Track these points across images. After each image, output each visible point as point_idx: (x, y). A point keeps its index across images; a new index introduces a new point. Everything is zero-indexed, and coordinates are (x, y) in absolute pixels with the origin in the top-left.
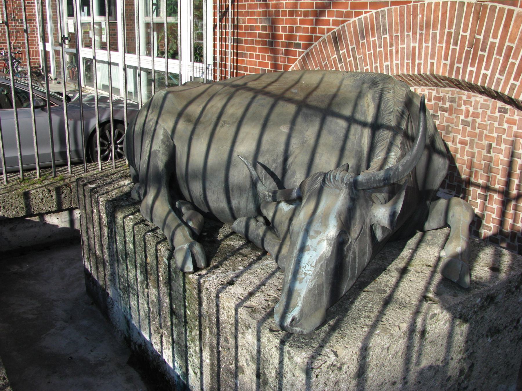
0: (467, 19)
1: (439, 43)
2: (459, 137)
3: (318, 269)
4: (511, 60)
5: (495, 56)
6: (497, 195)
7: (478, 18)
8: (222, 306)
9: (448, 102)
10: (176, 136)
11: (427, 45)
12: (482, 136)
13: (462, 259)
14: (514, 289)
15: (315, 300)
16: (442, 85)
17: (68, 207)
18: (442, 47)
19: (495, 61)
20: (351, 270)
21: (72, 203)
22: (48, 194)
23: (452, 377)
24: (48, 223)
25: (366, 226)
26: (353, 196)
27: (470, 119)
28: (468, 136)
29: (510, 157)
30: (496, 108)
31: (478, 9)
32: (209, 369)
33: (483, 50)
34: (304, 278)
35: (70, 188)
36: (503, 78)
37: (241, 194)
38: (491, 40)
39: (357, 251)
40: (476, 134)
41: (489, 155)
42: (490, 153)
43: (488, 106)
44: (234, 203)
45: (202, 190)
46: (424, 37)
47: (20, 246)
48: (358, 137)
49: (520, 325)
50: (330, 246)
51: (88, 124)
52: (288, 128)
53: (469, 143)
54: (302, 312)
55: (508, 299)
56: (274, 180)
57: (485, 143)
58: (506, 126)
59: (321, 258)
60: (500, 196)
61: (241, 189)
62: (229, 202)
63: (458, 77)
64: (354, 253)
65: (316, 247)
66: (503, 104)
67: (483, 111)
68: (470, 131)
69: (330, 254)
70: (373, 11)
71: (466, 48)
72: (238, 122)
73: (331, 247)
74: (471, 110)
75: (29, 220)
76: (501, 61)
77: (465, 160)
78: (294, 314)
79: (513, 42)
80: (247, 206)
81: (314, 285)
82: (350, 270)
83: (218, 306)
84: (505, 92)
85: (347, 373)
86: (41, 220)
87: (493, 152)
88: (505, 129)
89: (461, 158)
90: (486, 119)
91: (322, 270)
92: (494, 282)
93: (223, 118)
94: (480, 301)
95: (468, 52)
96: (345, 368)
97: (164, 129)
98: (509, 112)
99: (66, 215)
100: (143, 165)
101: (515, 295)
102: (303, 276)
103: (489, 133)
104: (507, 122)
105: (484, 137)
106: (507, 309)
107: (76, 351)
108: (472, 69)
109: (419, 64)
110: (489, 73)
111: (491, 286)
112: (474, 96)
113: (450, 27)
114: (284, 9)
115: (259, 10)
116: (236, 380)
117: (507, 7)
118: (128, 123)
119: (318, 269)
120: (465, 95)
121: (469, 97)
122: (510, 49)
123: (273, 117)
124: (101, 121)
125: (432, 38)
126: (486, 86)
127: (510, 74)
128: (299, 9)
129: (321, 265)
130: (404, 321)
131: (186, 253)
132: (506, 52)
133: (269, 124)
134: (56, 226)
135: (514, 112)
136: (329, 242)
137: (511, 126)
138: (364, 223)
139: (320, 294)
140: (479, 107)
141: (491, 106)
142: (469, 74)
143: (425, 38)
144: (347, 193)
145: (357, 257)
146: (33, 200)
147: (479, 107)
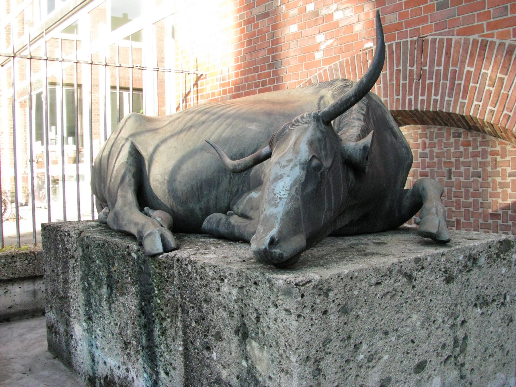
0: (412, 55)
3: (293, 192)
4: (457, 82)
5: (442, 81)
14: (495, 256)
23: (447, 346)
28: (428, 167)
33: (431, 78)
36: (452, 99)
39: (331, 180)
40: (435, 163)
41: (450, 180)
50: (304, 170)
53: (429, 173)
54: (280, 232)
57: (445, 170)
58: (462, 149)
67: (439, 140)
69: (304, 178)
76: (448, 84)
80: (216, 204)
81: (291, 208)
82: (326, 199)
84: (456, 111)
88: (462, 152)
90: (442, 147)
91: (297, 194)
96: (331, 295)
103: (447, 159)
104: (463, 145)
108: (423, 98)
110: (438, 98)
113: (398, 65)
117: (445, 37)
120: (420, 129)
129: (297, 189)
137: (466, 148)
140: (434, 137)
147: (434, 137)
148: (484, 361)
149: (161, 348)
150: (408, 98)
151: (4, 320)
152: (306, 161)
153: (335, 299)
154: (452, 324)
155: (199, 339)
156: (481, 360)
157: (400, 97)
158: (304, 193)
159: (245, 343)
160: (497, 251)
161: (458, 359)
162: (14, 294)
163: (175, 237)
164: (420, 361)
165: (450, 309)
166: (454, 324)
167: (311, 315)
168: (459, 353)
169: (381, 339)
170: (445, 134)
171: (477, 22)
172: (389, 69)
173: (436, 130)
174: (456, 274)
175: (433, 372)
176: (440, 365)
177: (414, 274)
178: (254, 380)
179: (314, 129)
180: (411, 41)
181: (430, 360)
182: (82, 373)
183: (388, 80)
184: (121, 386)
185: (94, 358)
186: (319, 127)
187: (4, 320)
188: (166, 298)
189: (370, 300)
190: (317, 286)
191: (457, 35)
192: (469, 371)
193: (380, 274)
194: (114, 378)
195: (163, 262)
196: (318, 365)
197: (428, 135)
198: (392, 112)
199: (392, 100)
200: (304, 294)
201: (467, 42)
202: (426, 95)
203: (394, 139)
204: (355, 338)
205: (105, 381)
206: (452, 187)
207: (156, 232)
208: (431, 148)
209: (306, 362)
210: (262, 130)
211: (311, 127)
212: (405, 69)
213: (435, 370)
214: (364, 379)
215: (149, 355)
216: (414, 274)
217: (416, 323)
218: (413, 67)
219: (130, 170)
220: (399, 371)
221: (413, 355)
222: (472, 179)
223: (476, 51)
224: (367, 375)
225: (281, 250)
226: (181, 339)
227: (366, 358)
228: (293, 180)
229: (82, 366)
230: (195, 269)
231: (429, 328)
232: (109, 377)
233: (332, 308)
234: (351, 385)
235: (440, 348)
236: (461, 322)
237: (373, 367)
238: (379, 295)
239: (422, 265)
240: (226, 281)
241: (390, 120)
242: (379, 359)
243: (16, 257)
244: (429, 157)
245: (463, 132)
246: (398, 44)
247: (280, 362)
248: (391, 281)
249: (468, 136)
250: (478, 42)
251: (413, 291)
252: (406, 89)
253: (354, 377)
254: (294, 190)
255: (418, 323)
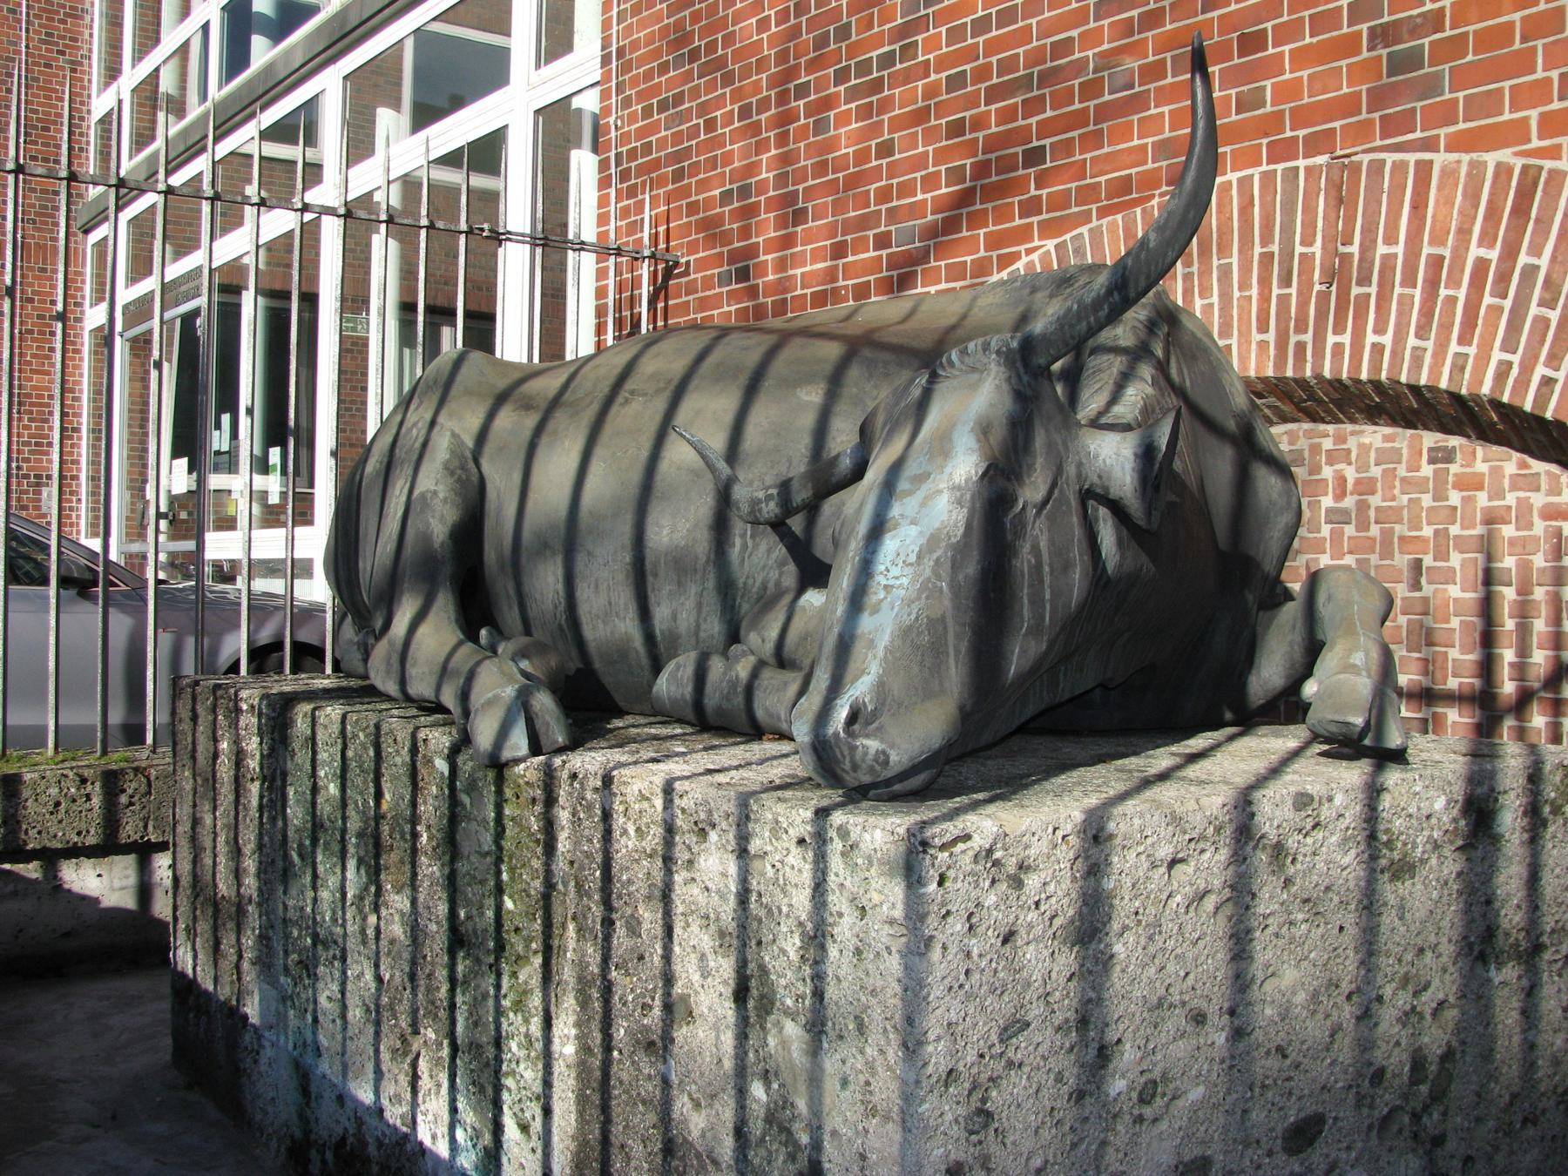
0: (1310, 210)
1: (1240, 289)
4: (1443, 292)
5: (1398, 290)
6: (1456, 710)
7: (1340, 201)
8: (621, 808)
10: (489, 449)
11: (1206, 301)
12: (1392, 543)
15: (921, 663)
17: (137, 837)
19: (1400, 303)
20: (1031, 603)
21: (150, 828)
22: (78, 789)
23: (1388, 1075)
24: (66, 886)
28: (1350, 552)
29: (1480, 587)
30: (1421, 454)
31: (1336, 178)
32: (572, 1082)
34: (886, 598)
35: (148, 778)
36: (1430, 345)
37: (679, 584)
38: (1382, 249)
39: (1043, 544)
40: (1373, 539)
41: (1417, 594)
42: (1420, 589)
43: (1398, 451)
44: (661, 614)
45: (560, 587)
46: (1196, 282)
51: (215, 650)
52: (820, 392)
54: (881, 688)
56: (782, 540)
57: (1402, 560)
58: (1455, 498)
59: (932, 542)
60: (1467, 709)
61: (681, 564)
62: (645, 613)
63: (1303, 369)
64: (1036, 550)
66: (1439, 436)
67: (1384, 471)
70: (1050, 244)
71: (1317, 287)
72: (672, 387)
73: (966, 510)
74: (1351, 474)
75: (9, 872)
78: (858, 693)
79: (1443, 243)
80: (698, 626)
81: (917, 618)
82: (1026, 601)
83: (607, 816)
85: (1042, 908)
86: (45, 876)
88: (1455, 508)
90: (1397, 491)
91: (939, 578)
93: (630, 385)
95: (1323, 298)
96: (1032, 882)
97: (454, 435)
98: (1459, 455)
99: (126, 868)
100: (385, 547)
102: (882, 595)
103: (1410, 529)
104: (1459, 486)
105: (1396, 545)
108: (1338, 339)
110: (1387, 339)
112: (1353, 433)
113: (1266, 239)
114: (799, 292)
115: (726, 309)
116: (665, 1061)
117: (1412, 158)
118: (337, 655)
119: (928, 572)
120: (1328, 436)
121: (1340, 439)
122: (1436, 262)
123: (779, 366)
124: (254, 641)
125: (1219, 280)
126: (1384, 376)
127: (1446, 328)
128: (841, 283)
129: (937, 561)
131: (509, 710)
132: (1426, 272)
133: (768, 383)
134: (91, 902)
135: (1474, 453)
136: (958, 494)
137: (1469, 497)
138: (1059, 470)
139: (937, 649)
141: (1405, 452)
143: (1200, 285)
144: (1003, 376)
145: (1047, 569)
146: (29, 804)
148: (1506, 1134)
149: (510, 1051)
153: (1043, 896)
154: (1408, 1007)
155: (626, 1017)
156: (1496, 1132)
158: (961, 577)
159: (763, 1028)
161: (1424, 1119)
163: (570, 721)
164: (1302, 1115)
165: (1400, 961)
166: (1414, 1008)
167: (966, 941)
168: (1428, 1101)
169: (1182, 1036)
171: (1511, 112)
172: (1240, 252)
174: (1423, 852)
175: (1344, 1155)
176: (1367, 1135)
177: (1291, 843)
178: (787, 1141)
180: (1307, 169)
181: (1334, 1114)
182: (270, 1130)
184: (384, 1167)
185: (308, 1085)
188: (533, 893)
189: (1152, 910)
190: (990, 852)
191: (1448, 149)
192: (1457, 1164)
193: (1185, 833)
194: (364, 1144)
195: (527, 783)
196: (984, 1100)
198: (1247, 382)
200: (948, 874)
201: (1477, 169)
204: (1100, 1025)
205: (336, 1155)
209: (947, 1085)
212: (1287, 253)
213: (1349, 1148)
214: (1126, 1154)
215: (472, 1071)
216: (1290, 841)
217: (1294, 993)
218: (1311, 244)
220: (1235, 1140)
221: (1282, 1096)
223: (1506, 200)
224: (1134, 1141)
225: (882, 741)
226: (572, 1019)
227: (1134, 1089)
228: (928, 535)
229: (270, 1109)
230: (621, 802)
231: (1335, 1013)
232: (350, 1140)
233: (1031, 926)
234: (1085, 1171)
235: (1367, 1081)
236: (1434, 1005)
237: (1155, 1120)
238: (1178, 898)
239: (1318, 815)
240: (713, 836)
242: (1174, 1098)
243: (93, 783)
246: (1268, 178)
247: (868, 1083)
248: (1217, 857)
250: (1510, 171)
251: (1285, 896)
253: (1093, 1147)
254: (929, 563)
255: (1301, 997)
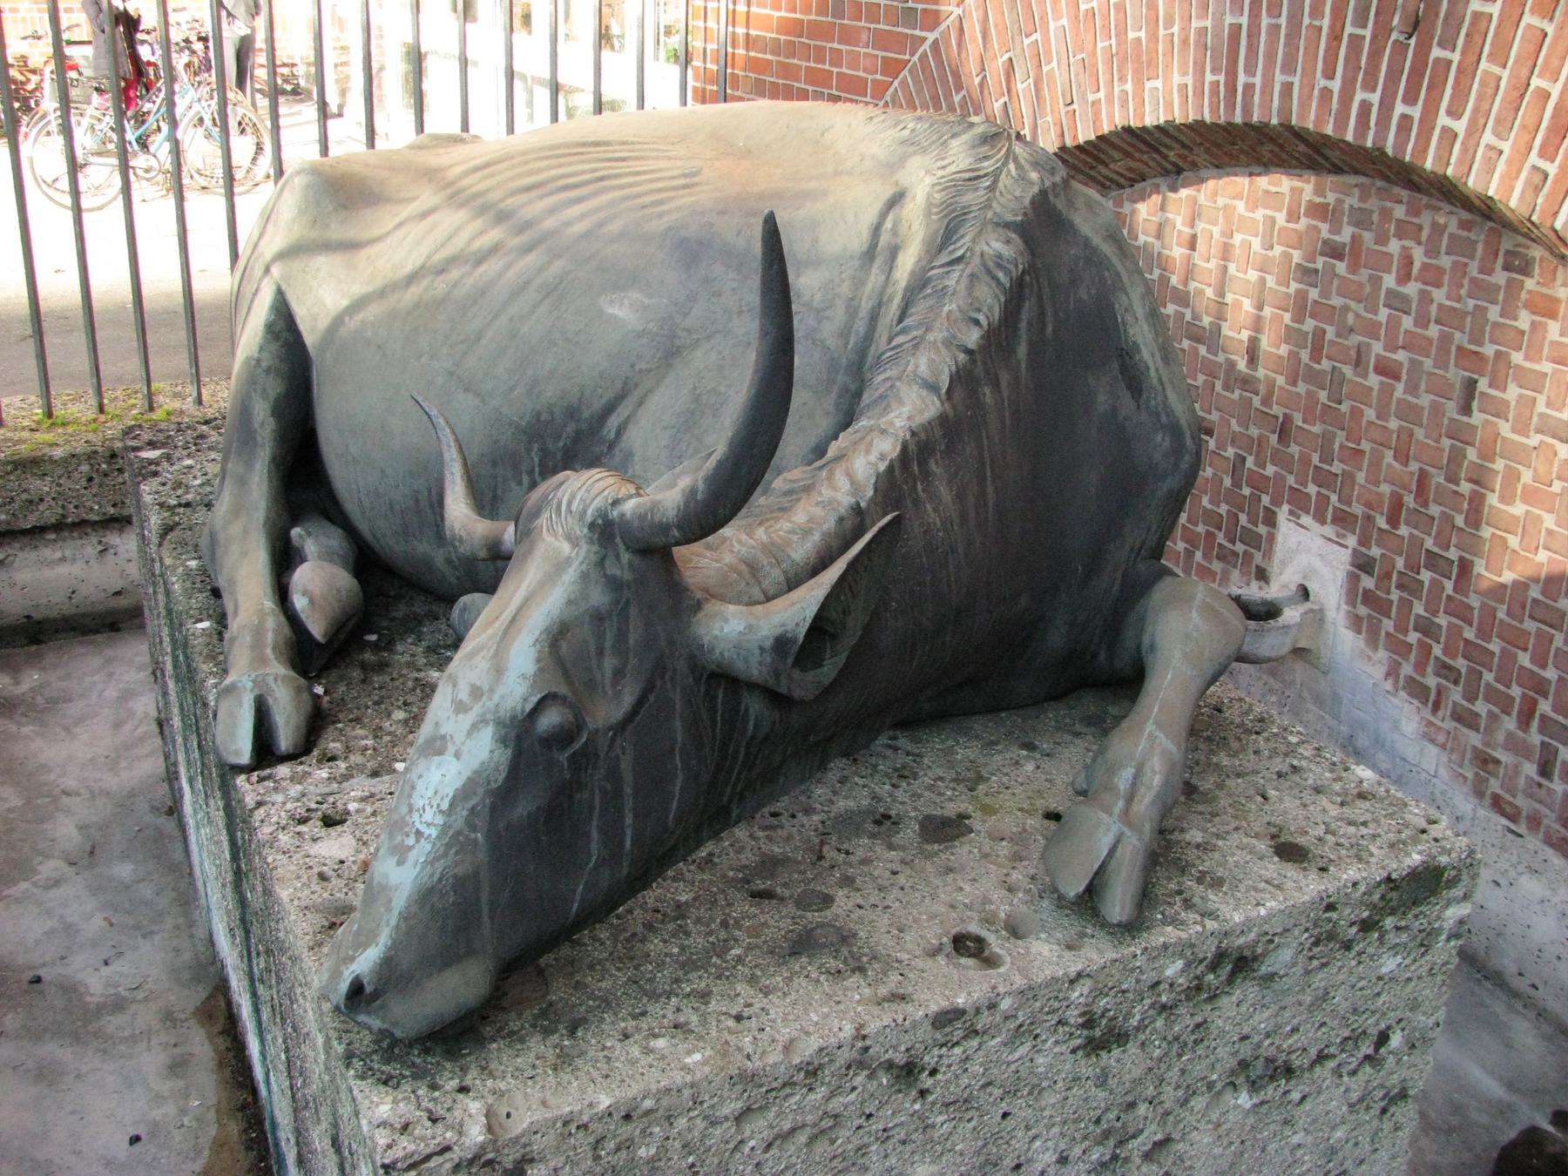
1: (1311, 15)
2: (1378, 348)
3: (459, 820)
4: (1536, 82)
5: (1483, 65)
9: (1348, 223)
11: (1273, 21)
12: (1448, 352)
13: (1126, 813)
16: (1327, 165)
18: (1320, 29)
19: (1483, 83)
25: (672, 679)
26: (618, 573)
27: (1412, 289)
28: (1403, 348)
39: (626, 766)
40: (1430, 340)
41: (1465, 419)
47: (28, 617)
48: (856, 343)
49: (1390, 1052)
50: (506, 747)
53: (1405, 371)
55: (1324, 965)
57: (1456, 375)
65: (463, 743)
68: (1411, 332)
69: (503, 775)
77: (1393, 432)
81: (440, 880)
82: (595, 834)
84: (1509, 200)
87: (1481, 411)
89: (1379, 422)
90: (1463, 292)
91: (473, 828)
92: (1258, 904)
94: (1182, 971)
101: (1359, 954)
103: (1470, 342)
105: (1453, 356)
106: (1325, 996)
107: (62, 958)
109: (1249, 88)
110: (1460, 126)
111: (1237, 918)
120: (1400, 202)
130: (937, 1003)
137: (1540, 323)
140: (1443, 249)
142: (1399, 128)
147: (1443, 249)
150: (1359, 96)
151: (104, 626)
152: (513, 718)
157: (1336, 85)
158: (501, 825)
160: (1366, 914)
162: (127, 556)
170: (1480, 247)
173: (1453, 226)
179: (584, 577)
183: (1307, 10)
186: (607, 564)
187: (104, 626)
193: (761, 1086)
197: (1425, 234)
199: (1306, 90)
202: (1420, 103)
203: (1127, 403)
206: (1468, 444)
207: (244, 687)
208: (1425, 283)
210: (651, 325)
211: (575, 565)
219: (264, 390)
222: (1535, 440)
241: (1129, 318)
244: (1413, 314)
245: (1542, 259)
248: (812, 1097)
249: (1555, 279)
252: (1358, 60)
